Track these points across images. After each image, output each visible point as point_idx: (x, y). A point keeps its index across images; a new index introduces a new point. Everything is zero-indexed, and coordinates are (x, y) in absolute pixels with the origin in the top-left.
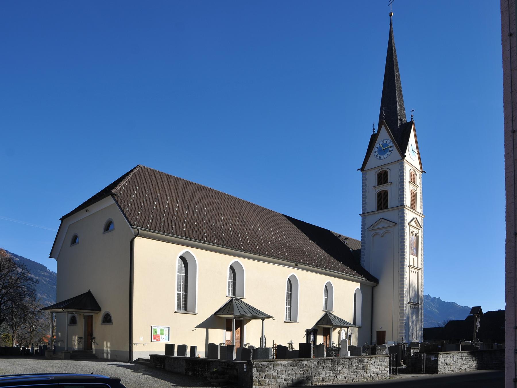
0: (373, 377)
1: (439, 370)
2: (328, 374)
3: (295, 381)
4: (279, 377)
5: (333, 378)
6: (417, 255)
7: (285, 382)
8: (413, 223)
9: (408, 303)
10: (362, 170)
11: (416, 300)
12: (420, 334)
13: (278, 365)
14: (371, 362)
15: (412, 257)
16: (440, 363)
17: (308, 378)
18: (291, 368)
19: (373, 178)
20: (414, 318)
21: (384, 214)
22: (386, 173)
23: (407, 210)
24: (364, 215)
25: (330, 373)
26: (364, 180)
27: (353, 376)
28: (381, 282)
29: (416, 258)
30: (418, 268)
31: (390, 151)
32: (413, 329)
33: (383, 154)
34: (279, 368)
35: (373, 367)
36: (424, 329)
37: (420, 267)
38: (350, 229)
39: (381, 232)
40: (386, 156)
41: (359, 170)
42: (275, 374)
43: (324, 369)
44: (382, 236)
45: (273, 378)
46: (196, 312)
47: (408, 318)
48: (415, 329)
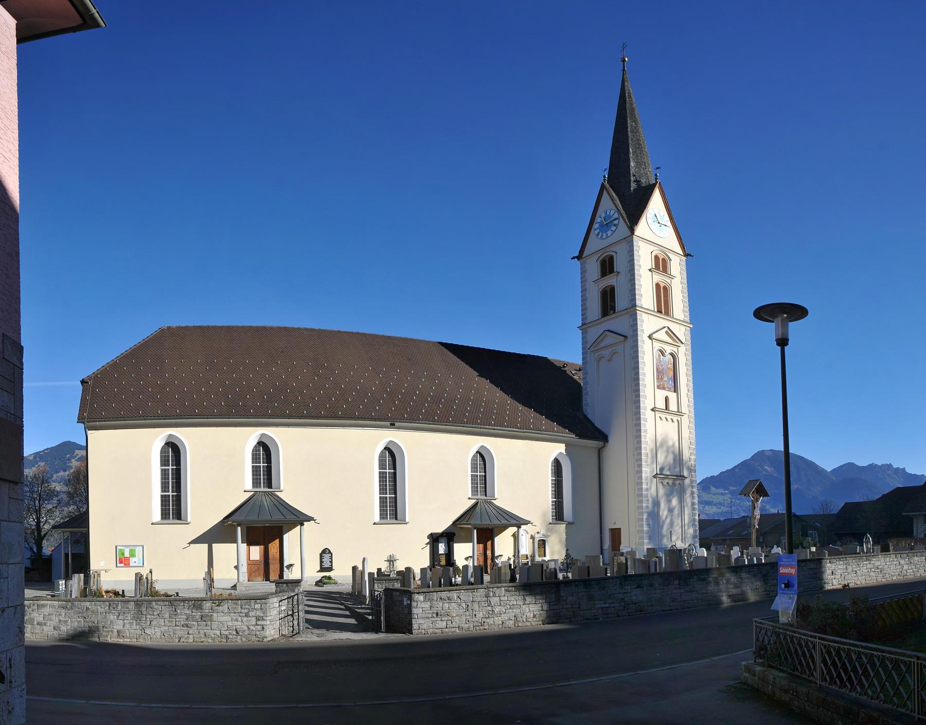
0: (227, 638)
1: (415, 626)
2: (128, 626)
3: (71, 632)
4: (45, 624)
5: (139, 632)
6: (676, 389)
7: (55, 632)
8: (662, 335)
9: (655, 477)
10: (579, 257)
11: (678, 469)
12: (691, 531)
13: (43, 606)
14: (221, 608)
15: (661, 394)
16: (415, 611)
17: (92, 631)
18: (63, 611)
19: (594, 267)
20: (675, 502)
21: (613, 323)
22: (611, 259)
23: (644, 315)
24: (584, 327)
25: (131, 624)
26: (583, 272)
27: (181, 632)
28: (611, 439)
29: (672, 396)
30: (679, 413)
31: (615, 225)
32: (672, 524)
33: (606, 232)
34: (47, 610)
35: (228, 618)
36: (700, 521)
37: (684, 409)
38: (565, 349)
39: (606, 353)
40: (609, 233)
41: (574, 258)
42: (41, 619)
43: (121, 617)
44: (609, 360)
45: (38, 624)
46: (282, 488)
47: (656, 504)
48: (678, 522)
